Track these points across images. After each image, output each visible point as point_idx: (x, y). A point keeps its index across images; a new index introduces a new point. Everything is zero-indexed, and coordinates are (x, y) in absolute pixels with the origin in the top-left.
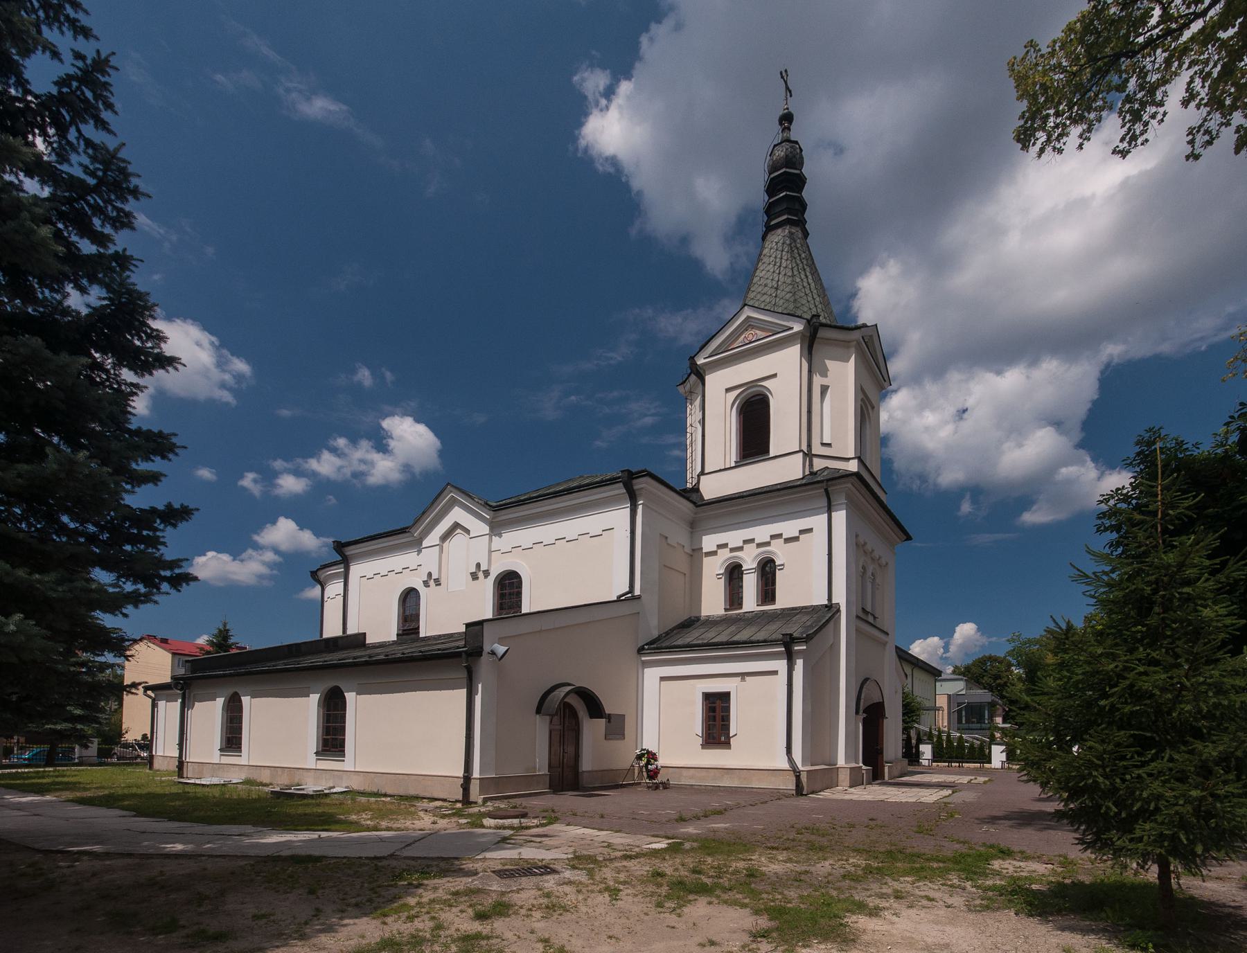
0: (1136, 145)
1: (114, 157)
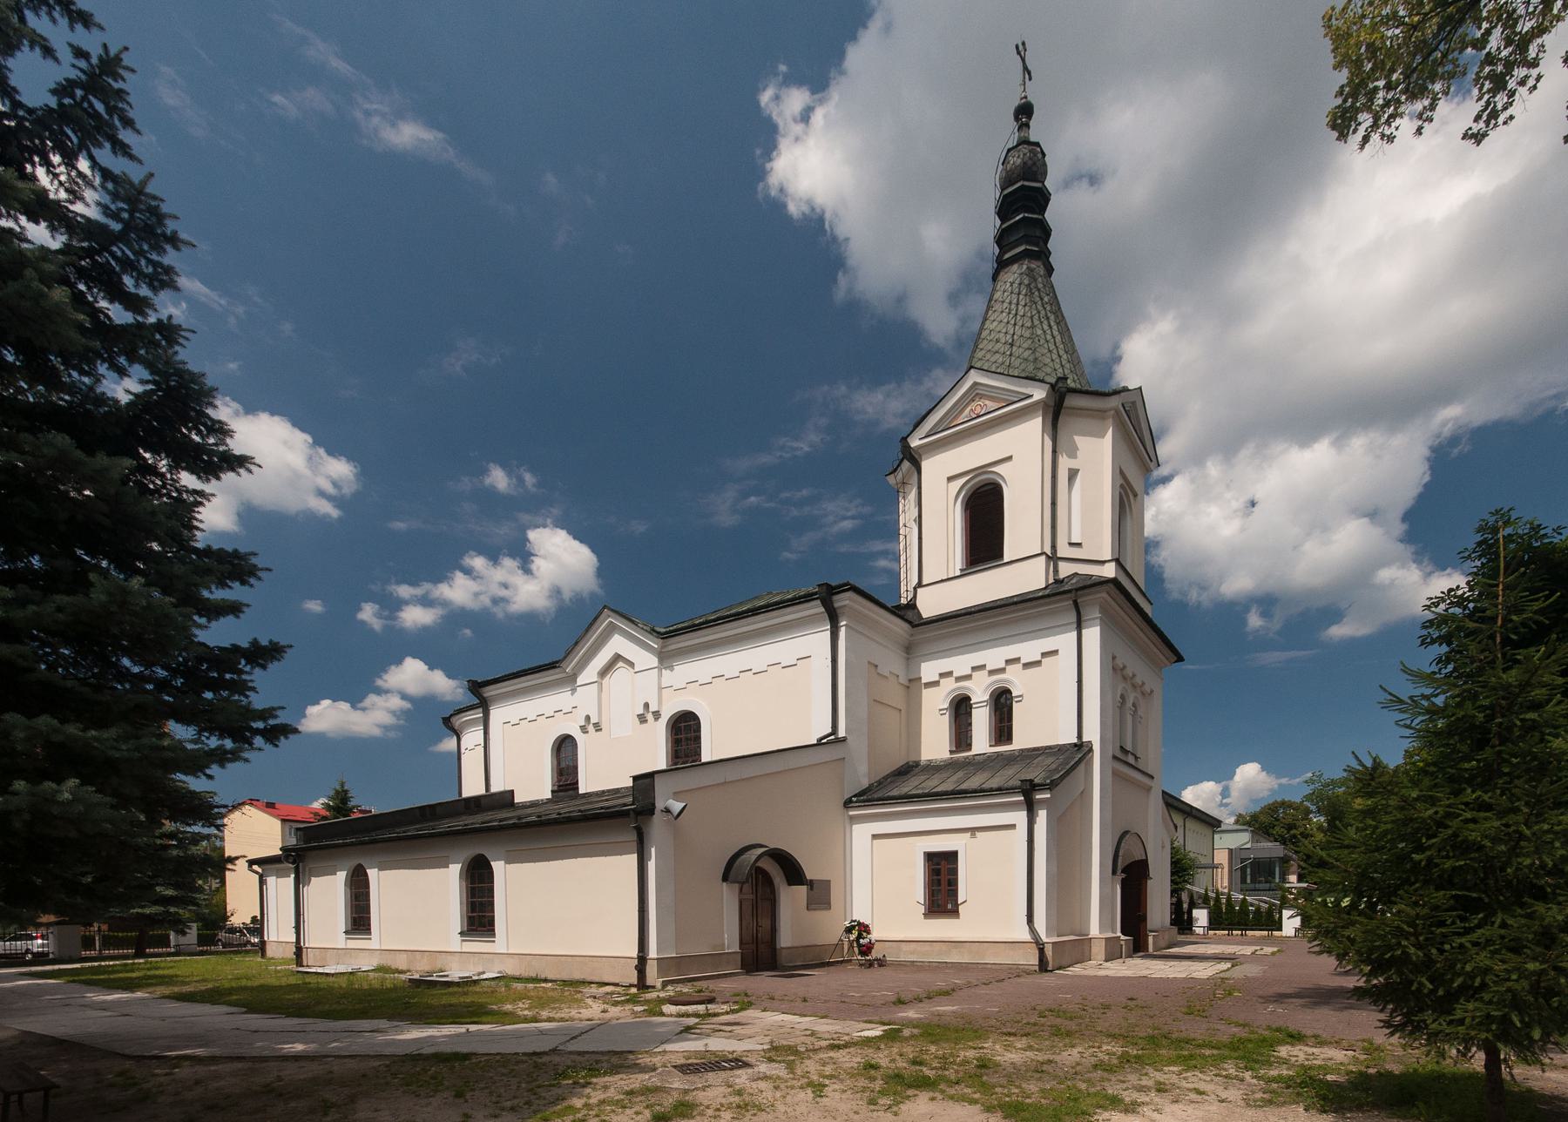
0: (1496, 125)
1: (141, 192)
